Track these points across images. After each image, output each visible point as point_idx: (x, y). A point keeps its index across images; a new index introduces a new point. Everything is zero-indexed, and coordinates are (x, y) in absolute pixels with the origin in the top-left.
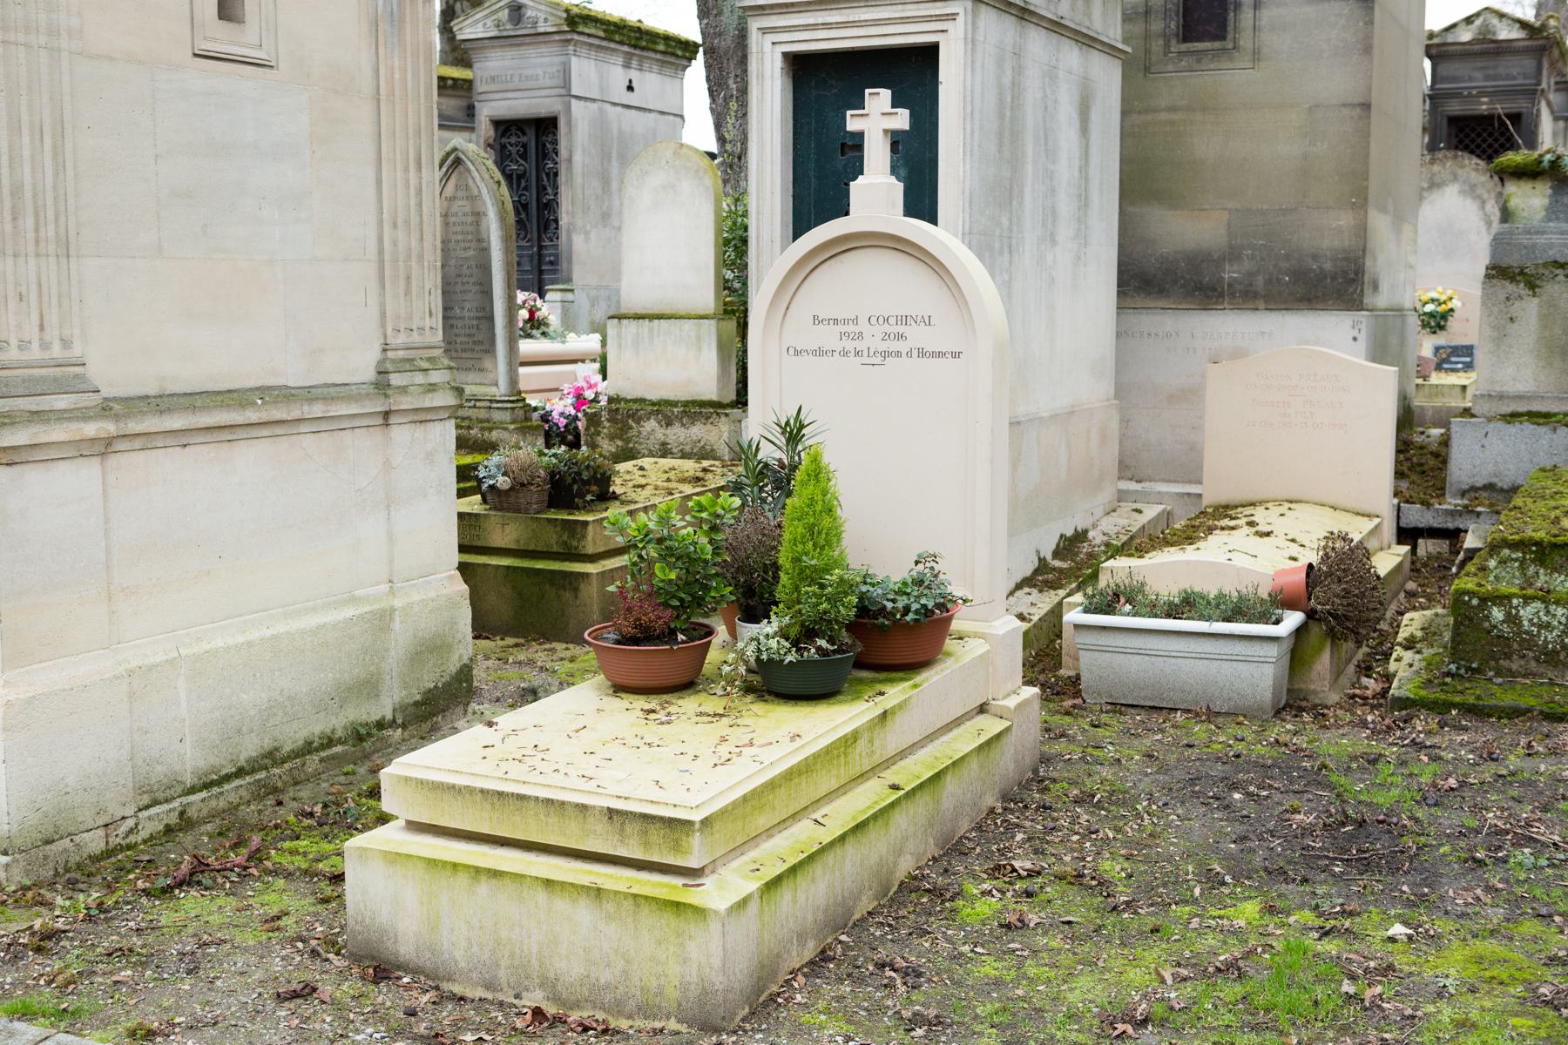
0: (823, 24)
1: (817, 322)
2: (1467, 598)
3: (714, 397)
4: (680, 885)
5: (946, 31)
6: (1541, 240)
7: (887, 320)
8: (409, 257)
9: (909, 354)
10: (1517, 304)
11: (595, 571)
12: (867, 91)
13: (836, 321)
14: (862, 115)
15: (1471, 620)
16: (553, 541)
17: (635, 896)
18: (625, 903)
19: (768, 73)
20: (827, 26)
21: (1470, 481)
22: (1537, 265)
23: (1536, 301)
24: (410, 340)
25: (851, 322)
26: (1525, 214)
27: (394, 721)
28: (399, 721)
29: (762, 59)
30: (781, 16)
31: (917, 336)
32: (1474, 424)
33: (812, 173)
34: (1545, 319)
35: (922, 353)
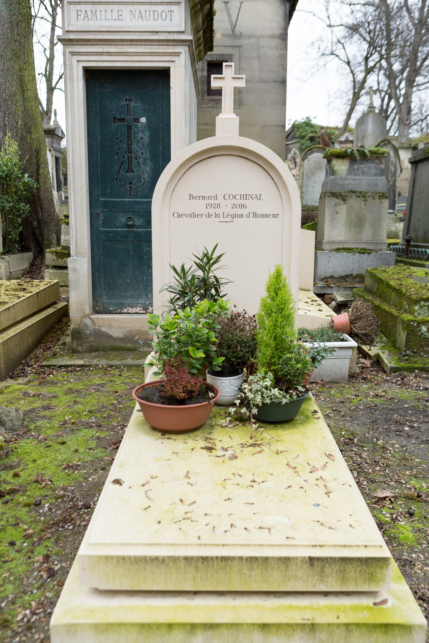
0: (107, 52)
1: (192, 198)
2: (412, 323)
4: (371, 604)
5: (174, 61)
6: (346, 182)
7: (234, 197)
9: (248, 216)
10: (339, 207)
13: (204, 198)
14: (220, 78)
15: (413, 332)
17: (347, 625)
18: (338, 631)
19: (75, 77)
20: (109, 54)
21: (324, 275)
22: (345, 192)
23: (345, 205)
25: (213, 198)
26: (340, 172)
29: (72, 69)
30: (82, 46)
32: (325, 253)
33: (98, 132)
35: (255, 215)
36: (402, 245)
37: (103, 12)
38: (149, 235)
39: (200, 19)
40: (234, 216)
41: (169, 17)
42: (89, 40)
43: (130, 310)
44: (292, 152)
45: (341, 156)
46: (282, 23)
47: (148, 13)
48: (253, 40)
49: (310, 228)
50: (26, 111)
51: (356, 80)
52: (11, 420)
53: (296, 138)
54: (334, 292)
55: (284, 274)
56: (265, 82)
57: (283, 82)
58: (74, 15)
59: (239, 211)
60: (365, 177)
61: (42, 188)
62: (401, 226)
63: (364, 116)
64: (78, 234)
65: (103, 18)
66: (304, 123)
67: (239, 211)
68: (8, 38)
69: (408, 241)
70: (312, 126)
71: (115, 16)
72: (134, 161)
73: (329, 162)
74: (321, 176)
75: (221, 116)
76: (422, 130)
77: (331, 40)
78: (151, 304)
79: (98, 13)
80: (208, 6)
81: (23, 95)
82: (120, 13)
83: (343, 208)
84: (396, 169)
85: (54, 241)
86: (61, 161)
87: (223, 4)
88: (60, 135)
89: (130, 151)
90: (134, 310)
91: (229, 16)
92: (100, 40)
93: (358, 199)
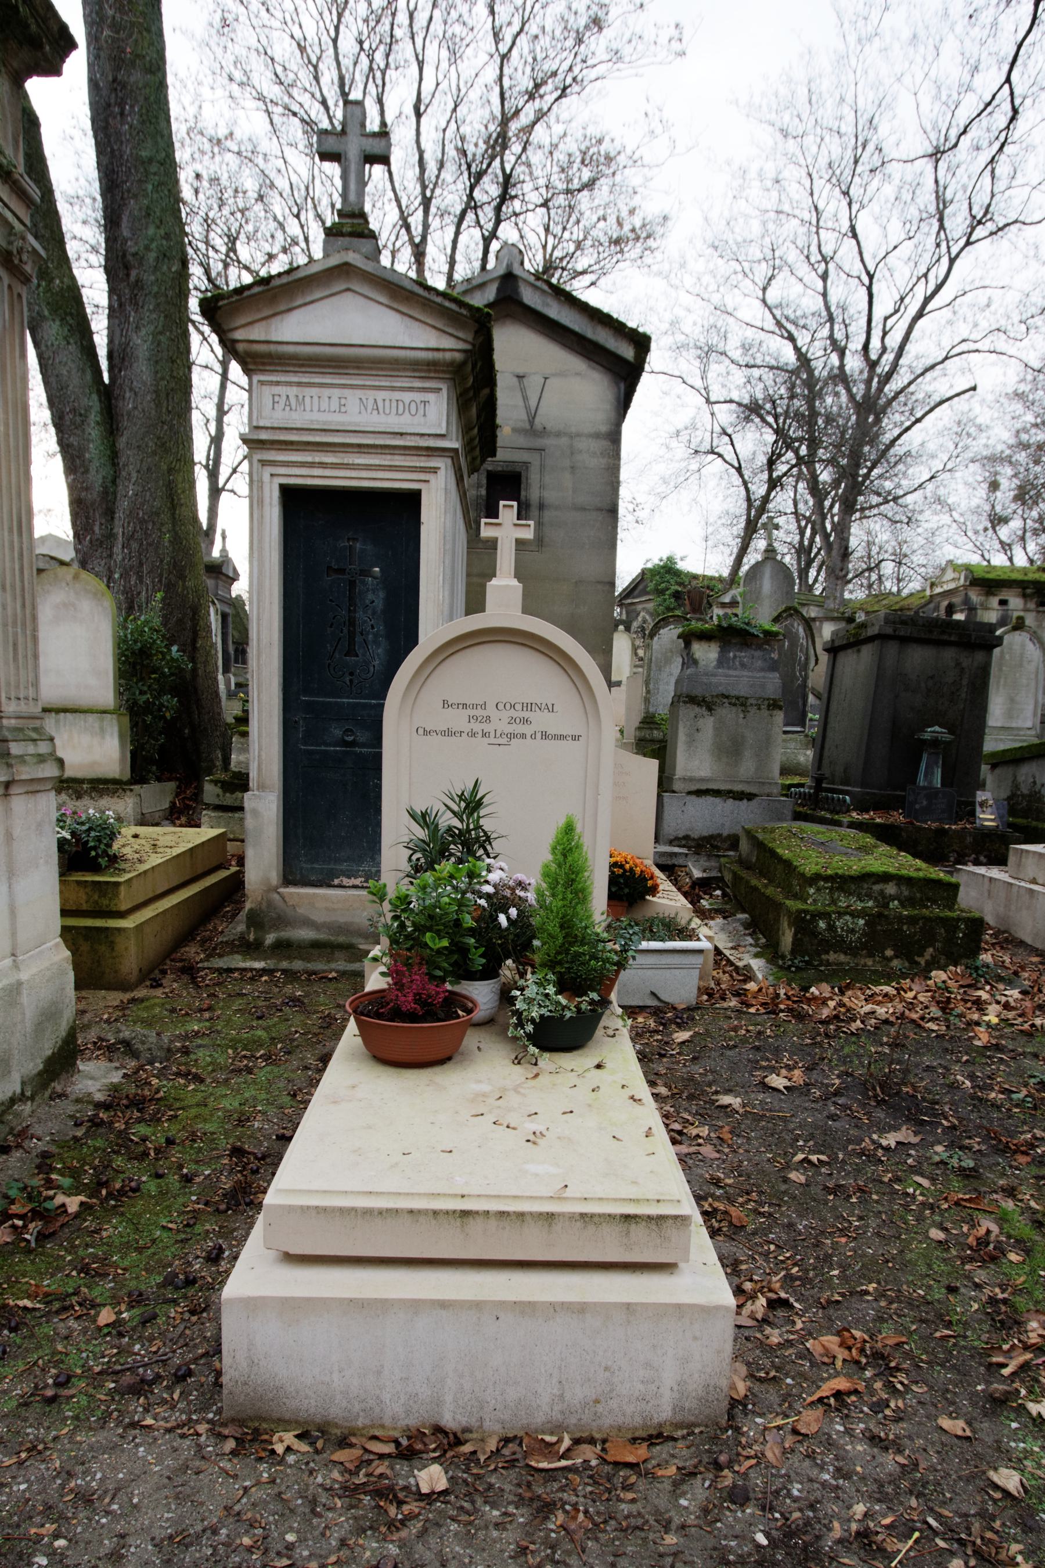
3: (117, 776)
6: (714, 680)
7: (513, 706)
8: (15, 623)
9: (533, 736)
11: (132, 925)
12: (502, 503)
16: (83, 902)
19: (267, 500)
20: (322, 465)
24: (19, 709)
27: (23, 1093)
28: (28, 1094)
31: (540, 721)
34: (717, 731)
35: (545, 736)
36: (810, 787)
37: (316, 399)
38: (378, 757)
39: (474, 411)
40: (512, 736)
41: (421, 411)
42: (292, 443)
43: (346, 881)
44: (640, 619)
45: (705, 636)
46: (613, 415)
47: (387, 403)
48: (564, 441)
49: (654, 755)
50: (177, 540)
51: (753, 497)
52: (150, 1049)
53: (648, 593)
54: (690, 864)
55: (578, 829)
56: (583, 509)
57: (613, 511)
58: (268, 401)
59: (520, 729)
60: (745, 673)
61: (200, 672)
62: (806, 756)
63: (756, 567)
64: (263, 754)
65: (316, 408)
66: (663, 567)
67: (520, 729)
68: (150, 418)
69: (818, 781)
70: (678, 573)
71: (335, 405)
72: (358, 639)
73: (688, 644)
74: (676, 667)
75: (494, 582)
76: (870, 586)
77: (709, 428)
78: (378, 872)
79: (307, 400)
80: (486, 391)
81: (173, 514)
82: (343, 401)
83: (708, 724)
84: (807, 659)
85: (219, 763)
86: (230, 619)
87: (515, 379)
88: (231, 575)
89: (352, 622)
90: (354, 881)
91: (525, 398)
92: (308, 443)
93: (734, 709)
